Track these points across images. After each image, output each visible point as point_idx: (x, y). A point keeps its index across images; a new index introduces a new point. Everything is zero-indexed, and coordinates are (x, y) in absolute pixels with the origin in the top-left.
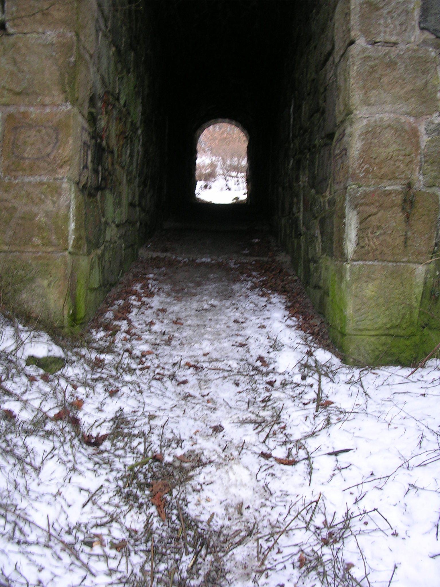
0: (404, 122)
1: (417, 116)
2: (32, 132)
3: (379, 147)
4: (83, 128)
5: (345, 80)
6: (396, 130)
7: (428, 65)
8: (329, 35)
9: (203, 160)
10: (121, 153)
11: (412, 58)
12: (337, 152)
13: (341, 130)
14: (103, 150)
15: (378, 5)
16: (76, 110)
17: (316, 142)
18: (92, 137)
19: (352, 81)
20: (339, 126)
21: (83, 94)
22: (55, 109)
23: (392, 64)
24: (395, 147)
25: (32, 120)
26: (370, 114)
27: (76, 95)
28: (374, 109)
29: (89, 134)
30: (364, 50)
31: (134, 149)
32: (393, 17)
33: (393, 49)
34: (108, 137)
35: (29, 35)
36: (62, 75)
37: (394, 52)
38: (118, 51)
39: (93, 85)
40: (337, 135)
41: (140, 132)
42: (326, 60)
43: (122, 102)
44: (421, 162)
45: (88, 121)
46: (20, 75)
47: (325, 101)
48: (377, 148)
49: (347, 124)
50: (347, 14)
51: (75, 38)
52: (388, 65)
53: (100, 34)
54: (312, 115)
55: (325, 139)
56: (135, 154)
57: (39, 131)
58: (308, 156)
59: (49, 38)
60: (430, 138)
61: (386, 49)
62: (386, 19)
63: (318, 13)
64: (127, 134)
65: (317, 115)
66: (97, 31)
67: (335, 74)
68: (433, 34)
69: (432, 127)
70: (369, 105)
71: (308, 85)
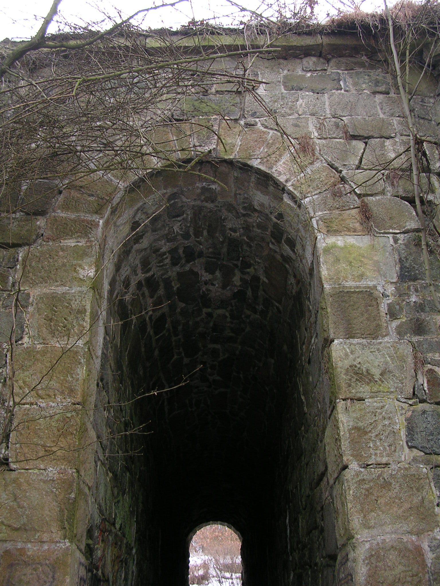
0: (407, 542)
1: (418, 534)
2: (28, 570)
3: (385, 570)
4: (80, 563)
5: (343, 504)
6: (400, 551)
7: (422, 481)
8: (321, 456)
9: (195, 559)
10: (116, 579)
11: (405, 476)
12: (342, 576)
13: (344, 553)
14: (99, 580)
15: (366, 429)
16: (74, 547)
17: (318, 560)
18: (89, 570)
19: (350, 505)
20: (341, 549)
21: (81, 529)
22: (53, 546)
23: (387, 485)
24: (401, 568)
25: (29, 557)
26: (371, 537)
27: (75, 532)
28: (374, 532)
29: (86, 567)
30: (357, 474)
31: (129, 570)
32: (381, 440)
33: (386, 469)
34: (104, 566)
35: (30, 471)
36: (61, 511)
37: (387, 472)
38: (115, 476)
39: (92, 517)
40: (339, 558)
41: (134, 551)
42: (320, 479)
43: (118, 526)
44: (429, 580)
45: (84, 554)
46: (19, 510)
47: (323, 520)
48: (383, 572)
49: (349, 548)
50: (338, 440)
51: (75, 475)
52: (383, 487)
53: (99, 463)
54: (311, 531)
55: (327, 559)
56: (130, 577)
57: (35, 569)
58: (310, 573)
59: (50, 475)
60: (435, 555)
61: (379, 471)
62: (375, 442)
63: (307, 431)
64: (122, 557)
65: (316, 533)
66: (96, 462)
67: (331, 495)
68: (421, 451)
69: (435, 543)
70: (369, 528)
71: (303, 500)
